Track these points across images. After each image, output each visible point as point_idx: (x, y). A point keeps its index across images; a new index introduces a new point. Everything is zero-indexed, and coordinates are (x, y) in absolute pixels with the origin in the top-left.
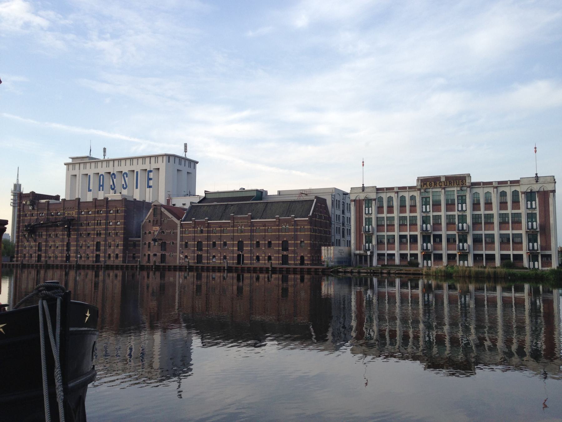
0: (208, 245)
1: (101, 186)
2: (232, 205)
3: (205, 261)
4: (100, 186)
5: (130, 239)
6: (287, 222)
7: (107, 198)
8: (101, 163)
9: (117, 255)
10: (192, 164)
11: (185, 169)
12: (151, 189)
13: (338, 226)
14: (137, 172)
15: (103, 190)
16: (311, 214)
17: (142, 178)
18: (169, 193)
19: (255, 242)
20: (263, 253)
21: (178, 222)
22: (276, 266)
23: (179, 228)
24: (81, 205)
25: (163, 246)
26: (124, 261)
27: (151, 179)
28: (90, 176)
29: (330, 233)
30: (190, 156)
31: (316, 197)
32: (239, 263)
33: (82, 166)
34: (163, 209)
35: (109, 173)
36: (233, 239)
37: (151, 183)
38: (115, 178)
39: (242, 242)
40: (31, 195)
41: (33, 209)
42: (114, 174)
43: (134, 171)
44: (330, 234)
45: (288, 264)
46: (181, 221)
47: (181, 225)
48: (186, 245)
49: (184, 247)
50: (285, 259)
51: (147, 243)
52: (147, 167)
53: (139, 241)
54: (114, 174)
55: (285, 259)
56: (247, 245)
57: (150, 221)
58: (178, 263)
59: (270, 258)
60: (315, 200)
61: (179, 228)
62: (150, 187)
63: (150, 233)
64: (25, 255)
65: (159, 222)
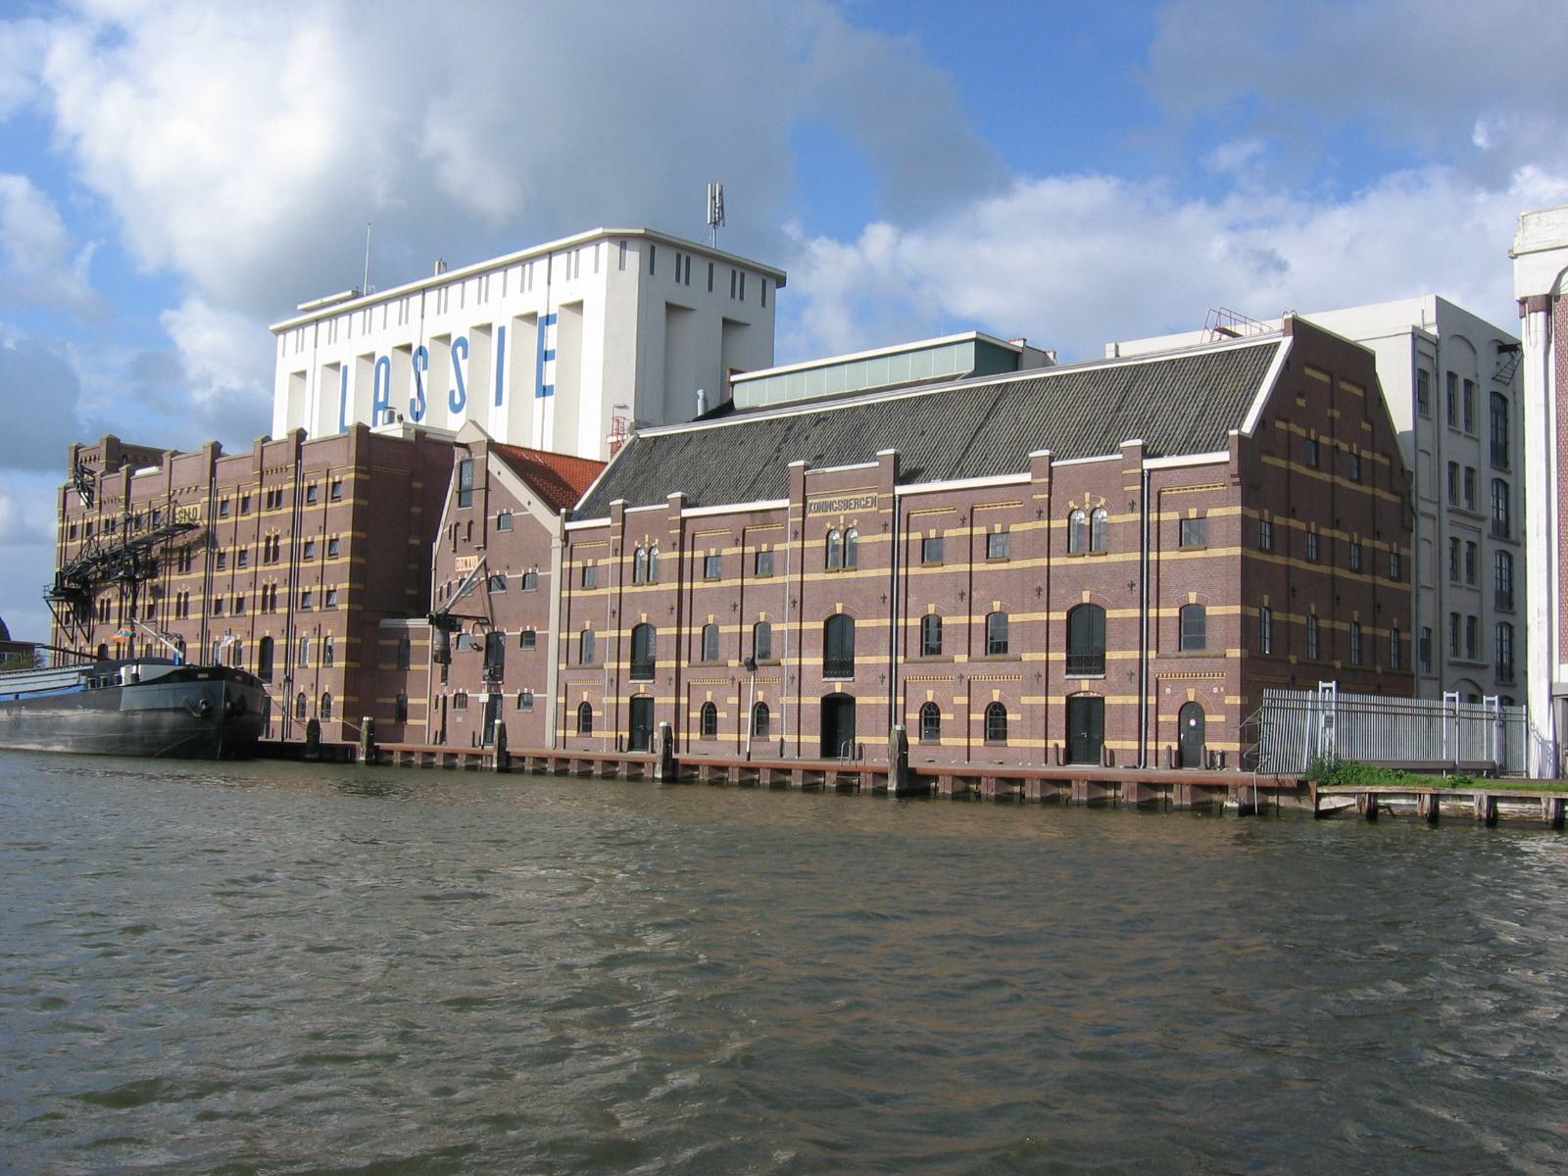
0: (1145, 633)
3: (1119, 744)
6: (1098, 481)
10: (753, 285)
11: (709, 302)
12: (550, 400)
13: (1465, 537)
14: (502, 331)
16: (1248, 427)
19: (914, 622)
20: (957, 684)
21: (551, 522)
28: (345, 369)
29: (1403, 569)
31: (1301, 330)
32: (829, 748)
34: (496, 465)
35: (407, 348)
44: (1402, 576)
46: (569, 518)
47: (566, 535)
55: (1084, 723)
58: (549, 745)
59: (996, 722)
60: (1286, 342)
61: (556, 555)
62: (544, 391)
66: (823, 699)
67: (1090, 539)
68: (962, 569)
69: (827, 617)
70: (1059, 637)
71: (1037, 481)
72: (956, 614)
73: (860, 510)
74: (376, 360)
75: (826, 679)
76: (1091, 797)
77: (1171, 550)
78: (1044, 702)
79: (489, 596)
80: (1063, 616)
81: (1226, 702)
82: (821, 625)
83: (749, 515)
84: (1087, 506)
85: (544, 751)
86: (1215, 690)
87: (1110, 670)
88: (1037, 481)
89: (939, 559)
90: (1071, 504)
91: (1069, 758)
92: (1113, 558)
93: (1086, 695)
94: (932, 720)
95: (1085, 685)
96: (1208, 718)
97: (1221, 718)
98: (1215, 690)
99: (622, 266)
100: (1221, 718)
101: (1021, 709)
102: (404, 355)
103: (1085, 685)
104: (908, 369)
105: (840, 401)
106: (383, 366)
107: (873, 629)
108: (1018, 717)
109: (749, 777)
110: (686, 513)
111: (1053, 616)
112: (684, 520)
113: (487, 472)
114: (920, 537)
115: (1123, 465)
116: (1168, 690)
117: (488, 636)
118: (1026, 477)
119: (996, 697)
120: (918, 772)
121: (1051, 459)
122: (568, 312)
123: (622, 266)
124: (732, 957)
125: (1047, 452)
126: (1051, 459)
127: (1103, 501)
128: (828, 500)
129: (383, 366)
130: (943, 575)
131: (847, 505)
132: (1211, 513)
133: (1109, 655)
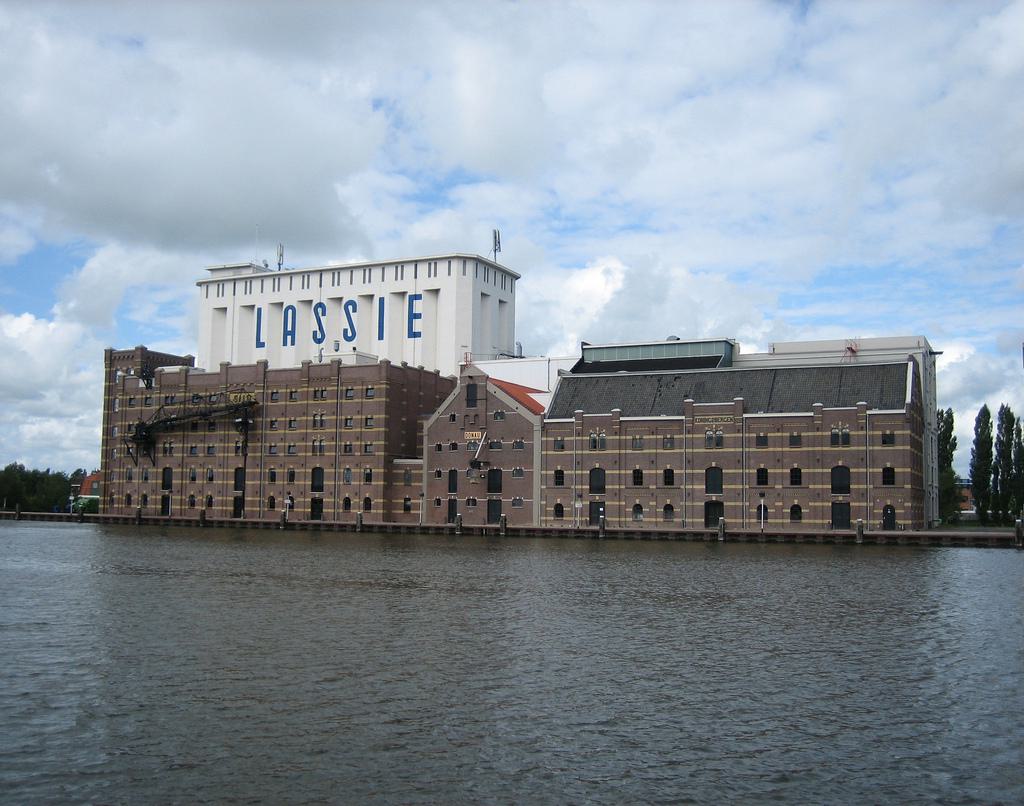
0: (182, 476)
1: (289, 335)
2: (677, 377)
4: (286, 333)
5: (396, 461)
7: (340, 362)
8: (426, 266)
9: (367, 501)
14: (382, 300)
15: (293, 343)
17: (396, 314)
18: (466, 350)
21: (535, 420)
22: (735, 530)
23: (537, 435)
24: (270, 377)
25: (494, 482)
26: (387, 517)
27: (418, 316)
28: (259, 310)
30: (502, 260)
33: (240, 286)
36: (690, 462)
37: (418, 325)
38: (324, 314)
39: (718, 470)
40: (139, 353)
41: (149, 386)
42: (320, 305)
43: (372, 296)
45: (848, 526)
46: (544, 416)
48: (559, 477)
49: (551, 482)
50: (841, 514)
51: (445, 471)
52: (315, 294)
53: (420, 467)
54: (320, 305)
56: (734, 479)
57: (453, 417)
62: (413, 334)
63: (454, 446)
64: (129, 497)
65: (482, 418)
66: (706, 503)
70: (161, 476)
74: (284, 307)
80: (310, 471)
87: (853, 492)
95: (841, 498)
99: (464, 274)
101: (808, 507)
102: (275, 310)
103: (317, 495)
104: (881, 358)
106: (290, 311)
111: (230, 470)
122: (393, 298)
123: (464, 274)
129: (290, 311)
130: (801, 452)
131: (716, 420)
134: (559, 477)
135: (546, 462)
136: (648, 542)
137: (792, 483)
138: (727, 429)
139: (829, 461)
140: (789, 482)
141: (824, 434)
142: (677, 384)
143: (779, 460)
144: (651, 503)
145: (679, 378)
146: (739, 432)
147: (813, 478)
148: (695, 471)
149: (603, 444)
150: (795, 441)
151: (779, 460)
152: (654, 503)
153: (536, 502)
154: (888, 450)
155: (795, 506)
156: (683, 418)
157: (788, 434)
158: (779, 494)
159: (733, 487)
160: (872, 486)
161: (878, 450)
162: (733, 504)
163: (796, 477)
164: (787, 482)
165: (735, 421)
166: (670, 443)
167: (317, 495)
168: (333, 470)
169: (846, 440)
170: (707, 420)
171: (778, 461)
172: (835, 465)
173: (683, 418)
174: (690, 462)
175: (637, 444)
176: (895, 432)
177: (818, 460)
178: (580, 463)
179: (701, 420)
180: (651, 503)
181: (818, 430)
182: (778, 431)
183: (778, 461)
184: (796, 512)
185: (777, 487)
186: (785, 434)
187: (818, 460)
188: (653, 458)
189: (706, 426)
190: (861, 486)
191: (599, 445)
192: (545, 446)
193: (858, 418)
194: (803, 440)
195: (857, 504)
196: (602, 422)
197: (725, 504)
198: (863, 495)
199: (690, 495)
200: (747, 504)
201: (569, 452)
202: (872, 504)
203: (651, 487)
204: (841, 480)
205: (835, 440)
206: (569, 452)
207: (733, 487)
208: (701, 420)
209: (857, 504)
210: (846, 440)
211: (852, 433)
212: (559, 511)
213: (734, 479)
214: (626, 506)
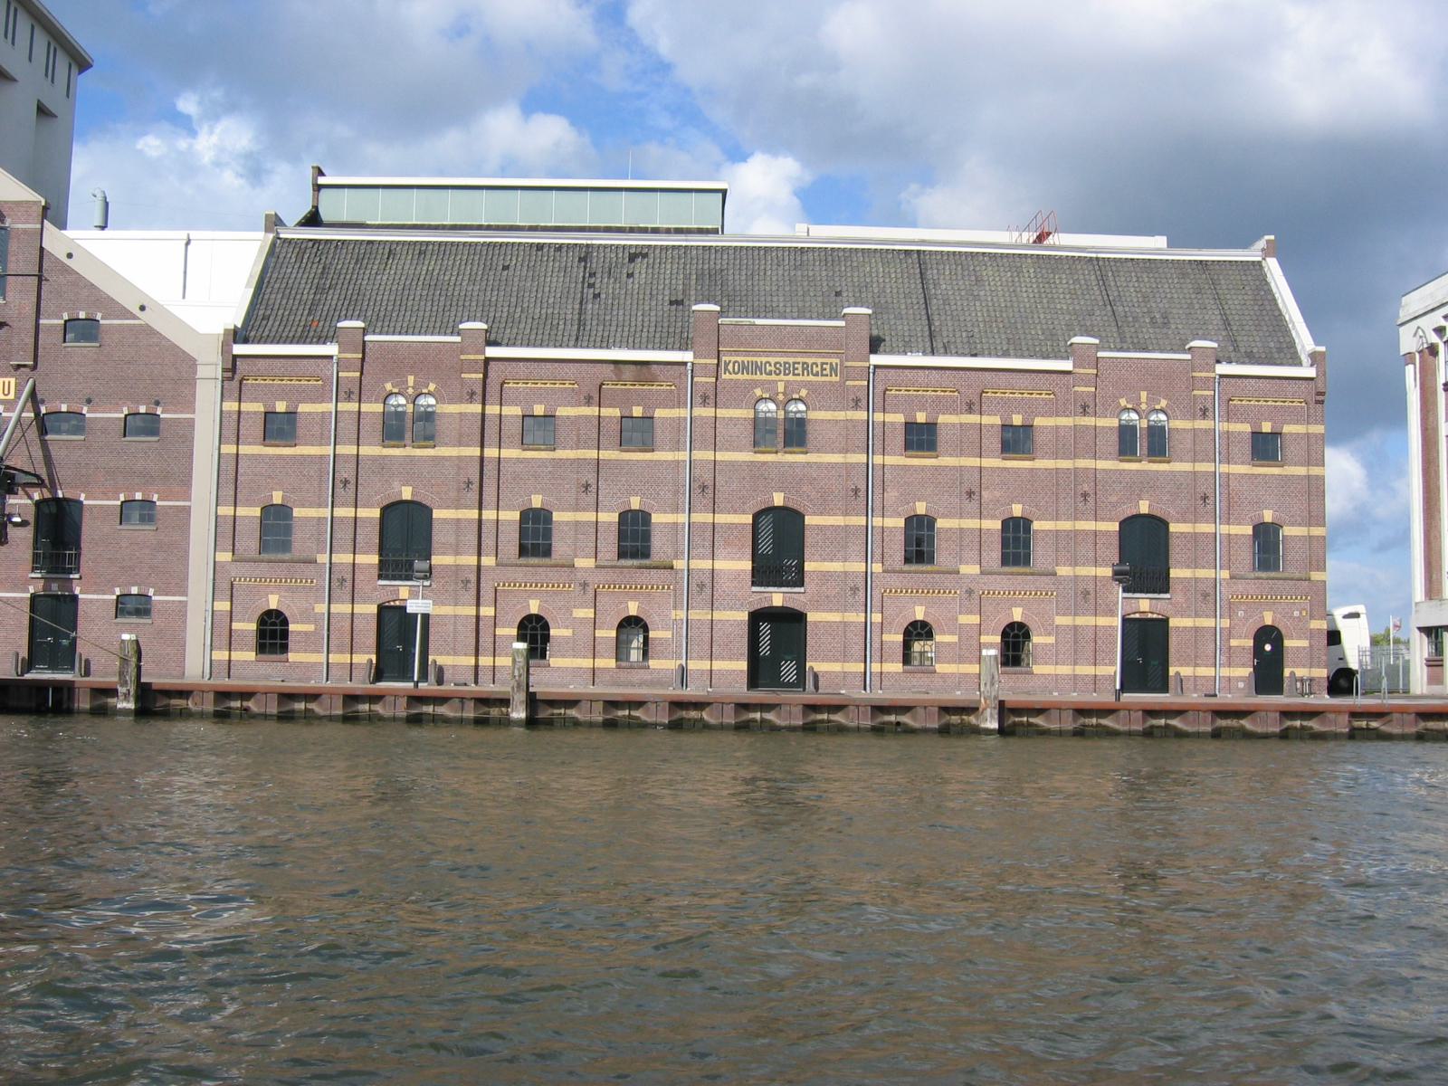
36: (707, 490)
48: (276, 524)
49: (249, 543)
55: (1146, 650)
67: (424, 427)
68: (246, 447)
69: (757, 510)
71: (1082, 371)
72: (458, 505)
73: (811, 378)
75: (754, 589)
76: (806, 721)
77: (1243, 463)
78: (482, 609)
79: (44, 445)
81: (1312, 627)
82: (748, 519)
83: (633, 367)
84: (410, 391)
85: (186, 681)
86: (1296, 613)
88: (1082, 371)
89: (429, 439)
90: (389, 386)
91: (379, 675)
92: (1040, 464)
93: (1143, 616)
94: (273, 634)
96: (1287, 643)
97: (1304, 643)
98: (1296, 613)
100: (1304, 643)
103: (1145, 604)
105: (356, 231)
107: (835, 528)
108: (567, 633)
109: (619, 716)
110: (492, 352)
111: (363, 513)
112: (487, 361)
113: (42, 249)
114: (619, 415)
115: (461, 349)
116: (1241, 613)
117: (38, 504)
118: (1067, 365)
119: (1017, 615)
120: (154, 687)
121: (365, 331)
124: (652, 952)
125: (360, 324)
126: (365, 331)
127: (432, 387)
128: (759, 360)
132: (659, 413)
133: (1174, 573)
134: (276, 524)
135: (232, 480)
136: (1319, 742)
137: (1005, 561)
138: (819, 396)
139: (1114, 499)
140: (996, 554)
141: (1101, 422)
142: (640, 266)
143: (972, 493)
144: (964, 619)
145: (645, 256)
146: (856, 404)
147: (1070, 545)
148: (721, 518)
149: (424, 427)
150: (1016, 441)
151: (972, 493)
152: (975, 619)
153: (199, 602)
154: (923, 468)
155: (269, 613)
156: (687, 356)
157: (616, 412)
158: (970, 592)
159: (836, 566)
160: (1225, 574)
161: (993, 469)
162: (834, 617)
163: (1016, 543)
164: (994, 554)
165: (847, 374)
166: (637, 433)
167: (1145, 604)
168: (474, 514)
169: (1158, 444)
170: (758, 368)
171: (970, 494)
172: (1129, 513)
173: (687, 356)
174: (707, 490)
175: (539, 429)
176: (1287, 429)
177: (1086, 495)
178: (348, 483)
179: (744, 368)
180: (964, 619)
181: (1085, 411)
182: (970, 410)
183: (970, 494)
184: (1015, 642)
185: (964, 569)
186: (986, 420)
187: (1085, 495)
188: (347, 472)
189: (755, 384)
190: (1203, 573)
191: (1141, 446)
192: (232, 429)
193: (1193, 383)
194: (1039, 439)
195: (1187, 622)
196: (425, 363)
197: (811, 617)
198: (1205, 596)
199: (708, 589)
200: (877, 618)
201: (667, 456)
202: (1226, 623)
203: (964, 569)
204: (1144, 553)
205: (1126, 441)
206: (667, 456)
207: (836, 566)
208: (744, 368)
209: (1187, 622)
210: (1158, 444)
211: (813, 415)
212: (273, 633)
213: (838, 541)
214: (1229, 633)
